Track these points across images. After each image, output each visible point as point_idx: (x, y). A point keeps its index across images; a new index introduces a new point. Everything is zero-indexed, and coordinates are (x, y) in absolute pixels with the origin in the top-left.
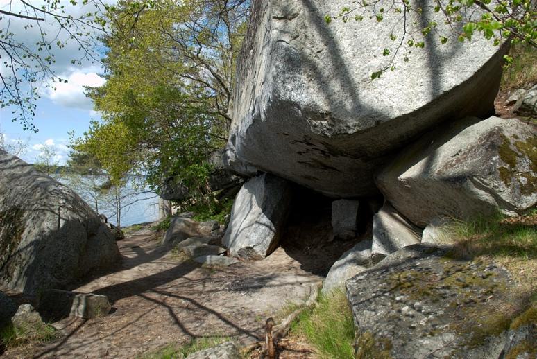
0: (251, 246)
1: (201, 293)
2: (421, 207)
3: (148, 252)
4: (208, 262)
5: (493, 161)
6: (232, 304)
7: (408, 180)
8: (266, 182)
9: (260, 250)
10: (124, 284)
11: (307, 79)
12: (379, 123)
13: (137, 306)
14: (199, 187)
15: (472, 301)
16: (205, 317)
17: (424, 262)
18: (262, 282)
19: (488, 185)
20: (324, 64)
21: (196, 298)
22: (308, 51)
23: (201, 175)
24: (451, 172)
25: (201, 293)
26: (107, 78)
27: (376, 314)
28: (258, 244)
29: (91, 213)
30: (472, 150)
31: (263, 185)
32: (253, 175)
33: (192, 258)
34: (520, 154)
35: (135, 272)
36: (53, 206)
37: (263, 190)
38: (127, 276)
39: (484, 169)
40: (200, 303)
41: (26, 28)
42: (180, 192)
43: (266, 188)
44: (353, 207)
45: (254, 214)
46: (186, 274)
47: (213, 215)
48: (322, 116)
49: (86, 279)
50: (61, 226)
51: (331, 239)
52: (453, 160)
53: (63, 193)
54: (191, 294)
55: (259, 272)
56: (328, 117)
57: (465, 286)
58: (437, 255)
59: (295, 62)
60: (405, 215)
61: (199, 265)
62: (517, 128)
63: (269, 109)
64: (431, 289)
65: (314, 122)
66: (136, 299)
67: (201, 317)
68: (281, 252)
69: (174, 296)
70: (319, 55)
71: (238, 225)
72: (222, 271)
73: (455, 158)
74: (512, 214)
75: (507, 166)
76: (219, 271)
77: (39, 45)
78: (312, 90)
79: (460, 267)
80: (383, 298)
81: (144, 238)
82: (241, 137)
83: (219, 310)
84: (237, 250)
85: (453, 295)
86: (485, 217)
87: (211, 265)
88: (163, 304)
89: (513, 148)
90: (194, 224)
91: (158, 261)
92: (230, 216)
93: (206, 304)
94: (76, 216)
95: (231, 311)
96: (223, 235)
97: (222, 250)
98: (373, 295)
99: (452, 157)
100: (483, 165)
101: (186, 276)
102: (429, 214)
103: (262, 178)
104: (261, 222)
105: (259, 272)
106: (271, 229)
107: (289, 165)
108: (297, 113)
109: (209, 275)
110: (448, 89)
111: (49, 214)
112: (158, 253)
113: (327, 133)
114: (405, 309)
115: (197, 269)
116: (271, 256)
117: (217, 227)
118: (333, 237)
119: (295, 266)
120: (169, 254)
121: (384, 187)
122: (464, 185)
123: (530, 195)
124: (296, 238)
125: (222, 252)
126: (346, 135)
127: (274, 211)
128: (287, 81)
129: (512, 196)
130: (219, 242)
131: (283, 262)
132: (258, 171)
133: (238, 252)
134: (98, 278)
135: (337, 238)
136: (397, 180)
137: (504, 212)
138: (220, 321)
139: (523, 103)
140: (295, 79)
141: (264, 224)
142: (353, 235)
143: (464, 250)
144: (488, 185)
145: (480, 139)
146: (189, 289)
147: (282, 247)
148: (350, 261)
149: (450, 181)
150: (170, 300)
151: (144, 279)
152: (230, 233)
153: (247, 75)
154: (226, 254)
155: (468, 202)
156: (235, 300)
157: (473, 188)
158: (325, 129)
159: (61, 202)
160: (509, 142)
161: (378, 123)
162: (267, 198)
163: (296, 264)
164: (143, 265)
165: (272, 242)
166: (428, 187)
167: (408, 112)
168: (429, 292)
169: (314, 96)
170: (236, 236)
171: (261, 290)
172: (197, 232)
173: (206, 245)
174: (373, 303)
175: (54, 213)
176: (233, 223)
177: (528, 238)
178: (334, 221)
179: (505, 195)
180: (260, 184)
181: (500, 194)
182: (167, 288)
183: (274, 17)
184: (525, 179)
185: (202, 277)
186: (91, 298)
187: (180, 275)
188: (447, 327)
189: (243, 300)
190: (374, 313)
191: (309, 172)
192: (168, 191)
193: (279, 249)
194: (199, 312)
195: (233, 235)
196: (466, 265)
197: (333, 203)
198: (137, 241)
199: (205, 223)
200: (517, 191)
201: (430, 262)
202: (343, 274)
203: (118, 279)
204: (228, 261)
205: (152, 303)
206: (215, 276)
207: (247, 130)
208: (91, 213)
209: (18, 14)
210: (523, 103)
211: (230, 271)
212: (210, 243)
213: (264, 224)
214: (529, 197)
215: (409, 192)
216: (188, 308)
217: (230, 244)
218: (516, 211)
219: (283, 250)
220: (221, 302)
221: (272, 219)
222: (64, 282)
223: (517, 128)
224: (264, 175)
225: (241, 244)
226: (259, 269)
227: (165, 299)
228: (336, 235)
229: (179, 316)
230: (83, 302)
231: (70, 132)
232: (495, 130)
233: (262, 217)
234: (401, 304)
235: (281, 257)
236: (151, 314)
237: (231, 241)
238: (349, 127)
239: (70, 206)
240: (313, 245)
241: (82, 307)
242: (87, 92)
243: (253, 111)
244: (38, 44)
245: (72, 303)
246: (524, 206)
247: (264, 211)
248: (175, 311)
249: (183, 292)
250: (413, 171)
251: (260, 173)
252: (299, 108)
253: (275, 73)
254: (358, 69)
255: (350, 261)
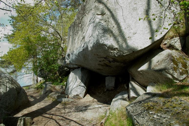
0: (78, 94)
1: (65, 113)
2: (145, 80)
3: (38, 98)
4: (63, 101)
5: (171, 65)
6: (78, 117)
7: (142, 71)
8: (82, 71)
9: (81, 96)
10: (34, 112)
11: (109, 36)
12: (134, 51)
13: (42, 120)
14: (54, 72)
15: (179, 113)
16: (70, 123)
17: (153, 99)
18: (85, 108)
19: (170, 72)
20: (115, 31)
21: (64, 115)
22: (109, 27)
23: (56, 68)
24: (157, 68)
25: (65, 113)
26: (13, 31)
27: (145, 119)
28: (80, 94)
29: (18, 84)
30: (163, 60)
31: (80, 72)
32: (76, 68)
33: (56, 100)
34: (179, 62)
35: (36, 106)
36: (4, 82)
37: (81, 73)
38: (34, 108)
39: (169, 67)
40: (66, 117)
41: (5, 14)
42: (45, 75)
43: (82, 73)
44: (113, 79)
45: (78, 82)
46: (56, 106)
47: (60, 83)
48: (115, 49)
49: (18, 111)
50: (8, 90)
51: (105, 90)
52: (157, 64)
53: (7, 77)
54: (61, 114)
55: (83, 104)
56: (117, 50)
57: (174, 107)
58: (157, 96)
59: (106, 31)
60: (139, 82)
61: (60, 102)
62: (175, 53)
63: (93, 46)
64: (162, 109)
65: (112, 51)
66: (40, 118)
67: (68, 123)
68: (88, 96)
69: (55, 115)
70: (113, 28)
71: (72, 87)
72: (69, 104)
73: (158, 63)
74: (178, 82)
75: (175, 66)
76: (68, 104)
77: (9, 21)
78: (111, 40)
79: (168, 101)
80: (144, 113)
81: (33, 92)
82: (75, 55)
83: (75, 119)
84: (73, 96)
85: (171, 111)
86: (170, 82)
87: (65, 102)
88: (52, 118)
89: (176, 60)
90: (54, 87)
91: (43, 101)
92: (67, 84)
93: (69, 118)
94: (13, 86)
95: (79, 119)
96: (65, 90)
97: (67, 96)
98: (140, 112)
99: (157, 63)
100: (168, 66)
101: (56, 107)
102: (148, 82)
103: (80, 69)
104: (81, 85)
105: (83, 104)
106: (85, 88)
107: (93, 65)
108: (105, 48)
109: (65, 106)
110: (155, 41)
111: (2, 86)
112: (42, 99)
113: (116, 55)
114: (155, 116)
115: (60, 104)
116: (85, 97)
117: (62, 87)
118: (106, 89)
119: (95, 101)
120: (46, 99)
121: (132, 73)
122: (162, 72)
123: (183, 75)
124: (93, 91)
125: (66, 97)
126: (122, 56)
127: (85, 81)
128: (102, 37)
129: (178, 76)
130: (64, 93)
131: (90, 99)
132: (78, 67)
133: (73, 97)
134: (23, 110)
135: (107, 90)
136: (137, 71)
137: (175, 81)
138: (76, 124)
139: (170, 44)
140: (105, 36)
141: (82, 86)
142: (113, 89)
143: (167, 95)
144: (170, 72)
145: (165, 57)
146: (59, 112)
147: (89, 94)
148: (121, 99)
149: (157, 71)
150: (54, 117)
151: (40, 109)
152: (68, 89)
153: (78, 33)
154: (68, 97)
155: (163, 78)
156: (79, 115)
157: (165, 73)
158: (115, 53)
159: (7, 81)
160: (175, 58)
161: (133, 52)
162: (83, 77)
163: (95, 100)
164: (38, 103)
165: (85, 92)
166: (149, 73)
167: (143, 48)
168: (161, 110)
169: (112, 42)
170: (71, 90)
171: (87, 111)
172: (55, 89)
173: (60, 94)
174: (142, 115)
175: (4, 85)
176: (69, 86)
177: (187, 90)
178: (106, 84)
179: (176, 75)
180: (79, 72)
181: (174, 75)
182: (51, 112)
183: (97, 14)
184: (181, 70)
185: (63, 107)
186: (26, 119)
187: (54, 106)
188: (174, 122)
189: (81, 115)
190: (143, 118)
191: (101, 67)
192: (41, 74)
193: (87, 95)
194: (68, 121)
195: (70, 90)
196: (170, 99)
197: (106, 78)
198: (30, 93)
199: (58, 86)
200: (179, 74)
201: (155, 99)
202: (119, 104)
203: (31, 110)
204: (71, 100)
205: (47, 119)
206: (67, 106)
207: (79, 53)
208: (18, 84)
209: (3, 8)
210: (170, 44)
211: (72, 104)
212: (61, 94)
213: (82, 86)
214: (183, 76)
215: (141, 75)
216: (62, 120)
217: (69, 94)
218: (179, 81)
219: (89, 95)
220: (74, 117)
221: (85, 84)
222: (9, 112)
223: (175, 53)
224: (80, 68)
225: (74, 93)
226: (82, 103)
227: (52, 117)
228: (107, 89)
229: (60, 123)
230: (23, 121)
231: (1, 52)
232: (169, 54)
233: (81, 84)
234: (152, 115)
235: (89, 98)
236: (48, 123)
237: (69, 92)
238: (124, 53)
239: (10, 82)
240: (99, 93)
241: (22, 123)
242: (4, 36)
243: (84, 46)
244: (8, 20)
245: (18, 121)
246: (181, 79)
247: (82, 81)
248: (58, 121)
249: (58, 113)
250: (144, 67)
251: (78, 68)
252: (107, 46)
253: (98, 34)
254: (127, 33)
255: (121, 99)
